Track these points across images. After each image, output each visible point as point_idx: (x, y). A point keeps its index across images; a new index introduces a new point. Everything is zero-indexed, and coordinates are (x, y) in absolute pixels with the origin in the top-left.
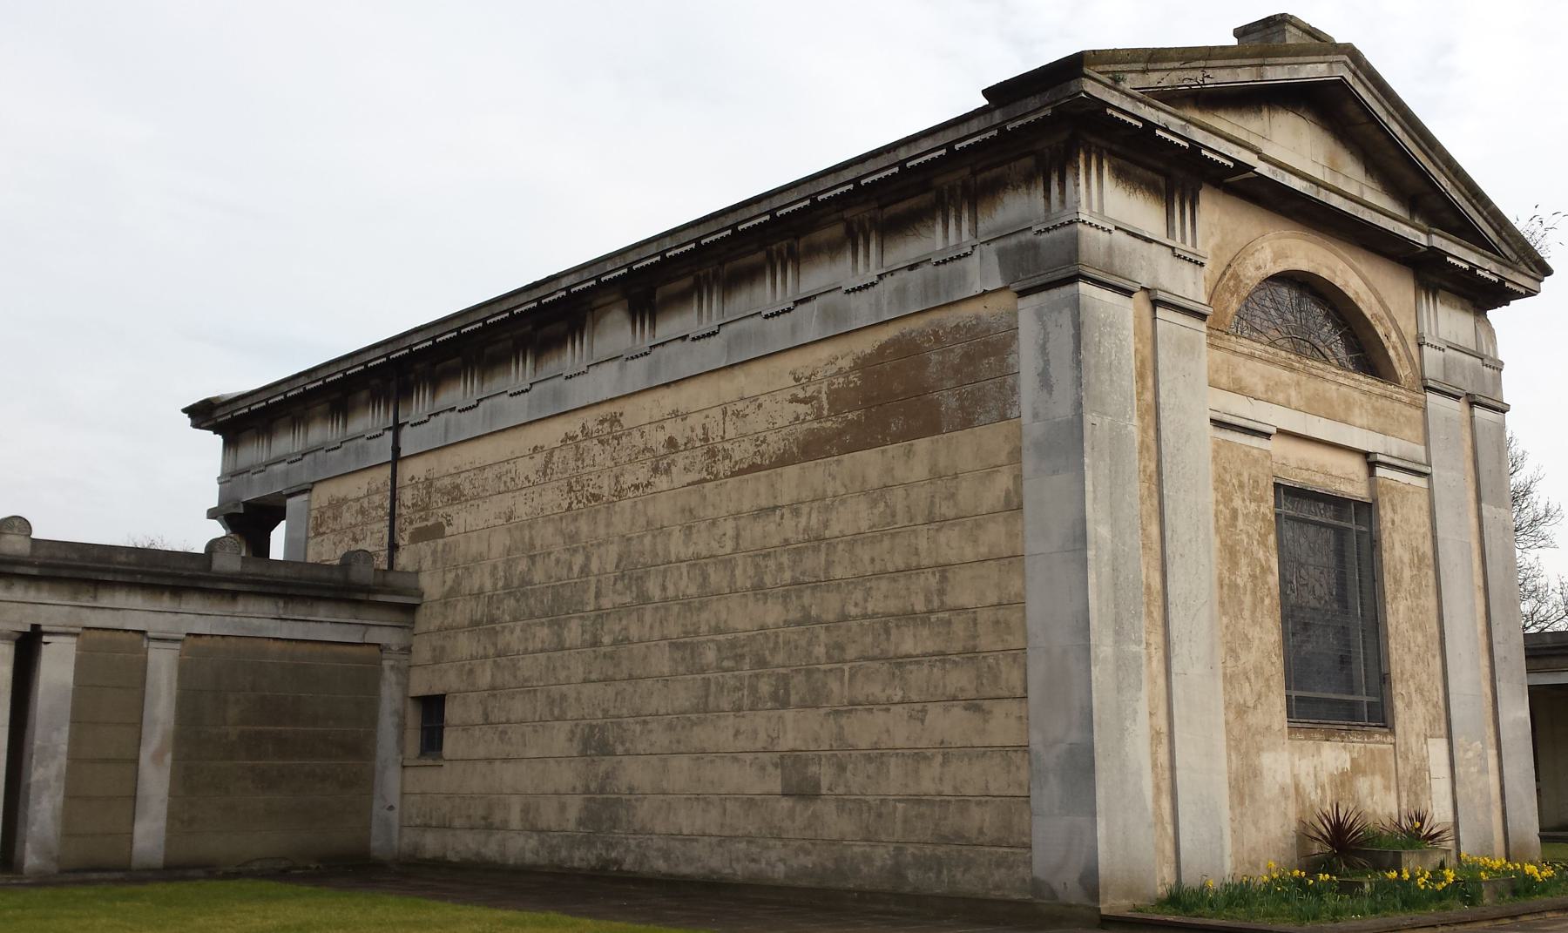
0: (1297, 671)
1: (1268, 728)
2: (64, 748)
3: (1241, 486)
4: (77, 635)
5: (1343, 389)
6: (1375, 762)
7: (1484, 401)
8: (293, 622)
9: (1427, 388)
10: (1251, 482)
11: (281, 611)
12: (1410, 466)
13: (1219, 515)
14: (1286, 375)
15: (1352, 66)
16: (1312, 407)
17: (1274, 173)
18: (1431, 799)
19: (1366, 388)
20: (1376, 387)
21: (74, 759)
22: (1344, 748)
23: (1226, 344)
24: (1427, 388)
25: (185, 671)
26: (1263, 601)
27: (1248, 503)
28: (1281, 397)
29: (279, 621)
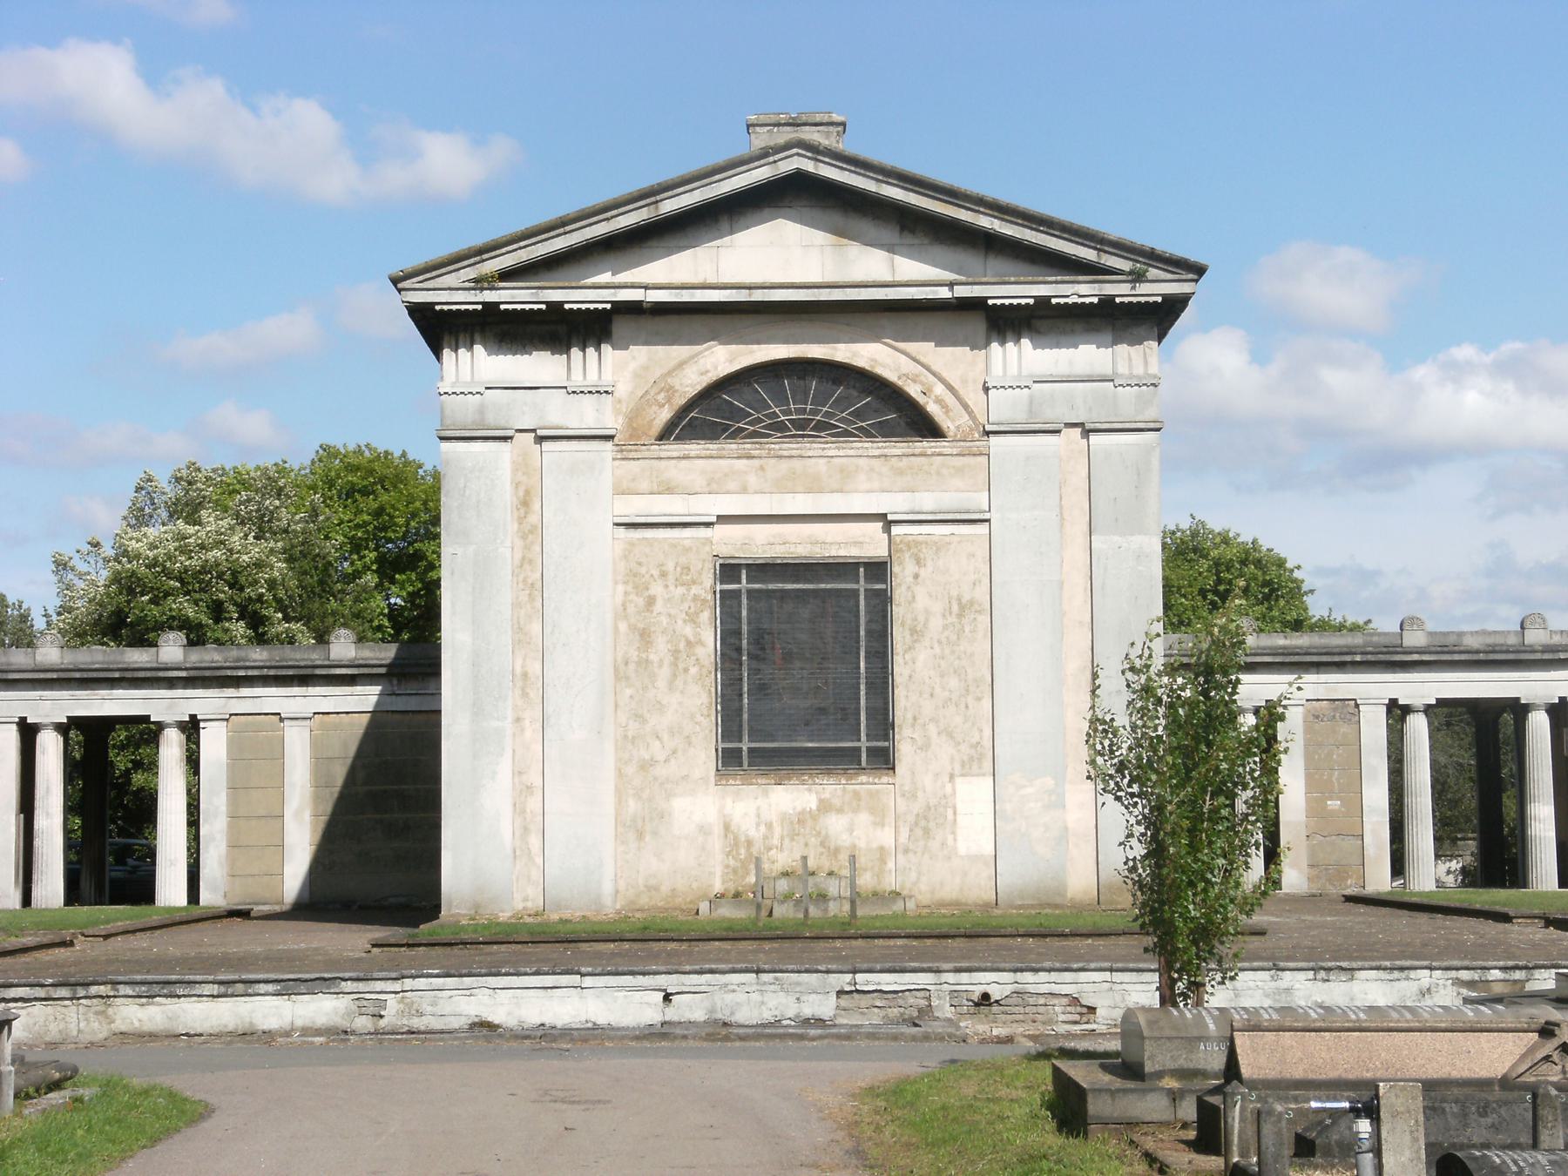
0: (730, 723)
1: (685, 778)
2: (224, 809)
3: (664, 575)
4: (227, 720)
5: (835, 460)
6: (859, 800)
7: (1098, 426)
8: (408, 697)
9: (988, 433)
10: (678, 569)
11: (396, 688)
12: (959, 517)
13: (628, 604)
14: (742, 464)
15: (809, 154)
16: (782, 486)
17: (676, 295)
18: (953, 833)
19: (877, 452)
20: (928, 445)
21: (233, 817)
22: (810, 790)
23: (647, 454)
24: (988, 433)
25: (316, 744)
26: (686, 670)
27: (672, 588)
28: (732, 485)
29: (394, 697)
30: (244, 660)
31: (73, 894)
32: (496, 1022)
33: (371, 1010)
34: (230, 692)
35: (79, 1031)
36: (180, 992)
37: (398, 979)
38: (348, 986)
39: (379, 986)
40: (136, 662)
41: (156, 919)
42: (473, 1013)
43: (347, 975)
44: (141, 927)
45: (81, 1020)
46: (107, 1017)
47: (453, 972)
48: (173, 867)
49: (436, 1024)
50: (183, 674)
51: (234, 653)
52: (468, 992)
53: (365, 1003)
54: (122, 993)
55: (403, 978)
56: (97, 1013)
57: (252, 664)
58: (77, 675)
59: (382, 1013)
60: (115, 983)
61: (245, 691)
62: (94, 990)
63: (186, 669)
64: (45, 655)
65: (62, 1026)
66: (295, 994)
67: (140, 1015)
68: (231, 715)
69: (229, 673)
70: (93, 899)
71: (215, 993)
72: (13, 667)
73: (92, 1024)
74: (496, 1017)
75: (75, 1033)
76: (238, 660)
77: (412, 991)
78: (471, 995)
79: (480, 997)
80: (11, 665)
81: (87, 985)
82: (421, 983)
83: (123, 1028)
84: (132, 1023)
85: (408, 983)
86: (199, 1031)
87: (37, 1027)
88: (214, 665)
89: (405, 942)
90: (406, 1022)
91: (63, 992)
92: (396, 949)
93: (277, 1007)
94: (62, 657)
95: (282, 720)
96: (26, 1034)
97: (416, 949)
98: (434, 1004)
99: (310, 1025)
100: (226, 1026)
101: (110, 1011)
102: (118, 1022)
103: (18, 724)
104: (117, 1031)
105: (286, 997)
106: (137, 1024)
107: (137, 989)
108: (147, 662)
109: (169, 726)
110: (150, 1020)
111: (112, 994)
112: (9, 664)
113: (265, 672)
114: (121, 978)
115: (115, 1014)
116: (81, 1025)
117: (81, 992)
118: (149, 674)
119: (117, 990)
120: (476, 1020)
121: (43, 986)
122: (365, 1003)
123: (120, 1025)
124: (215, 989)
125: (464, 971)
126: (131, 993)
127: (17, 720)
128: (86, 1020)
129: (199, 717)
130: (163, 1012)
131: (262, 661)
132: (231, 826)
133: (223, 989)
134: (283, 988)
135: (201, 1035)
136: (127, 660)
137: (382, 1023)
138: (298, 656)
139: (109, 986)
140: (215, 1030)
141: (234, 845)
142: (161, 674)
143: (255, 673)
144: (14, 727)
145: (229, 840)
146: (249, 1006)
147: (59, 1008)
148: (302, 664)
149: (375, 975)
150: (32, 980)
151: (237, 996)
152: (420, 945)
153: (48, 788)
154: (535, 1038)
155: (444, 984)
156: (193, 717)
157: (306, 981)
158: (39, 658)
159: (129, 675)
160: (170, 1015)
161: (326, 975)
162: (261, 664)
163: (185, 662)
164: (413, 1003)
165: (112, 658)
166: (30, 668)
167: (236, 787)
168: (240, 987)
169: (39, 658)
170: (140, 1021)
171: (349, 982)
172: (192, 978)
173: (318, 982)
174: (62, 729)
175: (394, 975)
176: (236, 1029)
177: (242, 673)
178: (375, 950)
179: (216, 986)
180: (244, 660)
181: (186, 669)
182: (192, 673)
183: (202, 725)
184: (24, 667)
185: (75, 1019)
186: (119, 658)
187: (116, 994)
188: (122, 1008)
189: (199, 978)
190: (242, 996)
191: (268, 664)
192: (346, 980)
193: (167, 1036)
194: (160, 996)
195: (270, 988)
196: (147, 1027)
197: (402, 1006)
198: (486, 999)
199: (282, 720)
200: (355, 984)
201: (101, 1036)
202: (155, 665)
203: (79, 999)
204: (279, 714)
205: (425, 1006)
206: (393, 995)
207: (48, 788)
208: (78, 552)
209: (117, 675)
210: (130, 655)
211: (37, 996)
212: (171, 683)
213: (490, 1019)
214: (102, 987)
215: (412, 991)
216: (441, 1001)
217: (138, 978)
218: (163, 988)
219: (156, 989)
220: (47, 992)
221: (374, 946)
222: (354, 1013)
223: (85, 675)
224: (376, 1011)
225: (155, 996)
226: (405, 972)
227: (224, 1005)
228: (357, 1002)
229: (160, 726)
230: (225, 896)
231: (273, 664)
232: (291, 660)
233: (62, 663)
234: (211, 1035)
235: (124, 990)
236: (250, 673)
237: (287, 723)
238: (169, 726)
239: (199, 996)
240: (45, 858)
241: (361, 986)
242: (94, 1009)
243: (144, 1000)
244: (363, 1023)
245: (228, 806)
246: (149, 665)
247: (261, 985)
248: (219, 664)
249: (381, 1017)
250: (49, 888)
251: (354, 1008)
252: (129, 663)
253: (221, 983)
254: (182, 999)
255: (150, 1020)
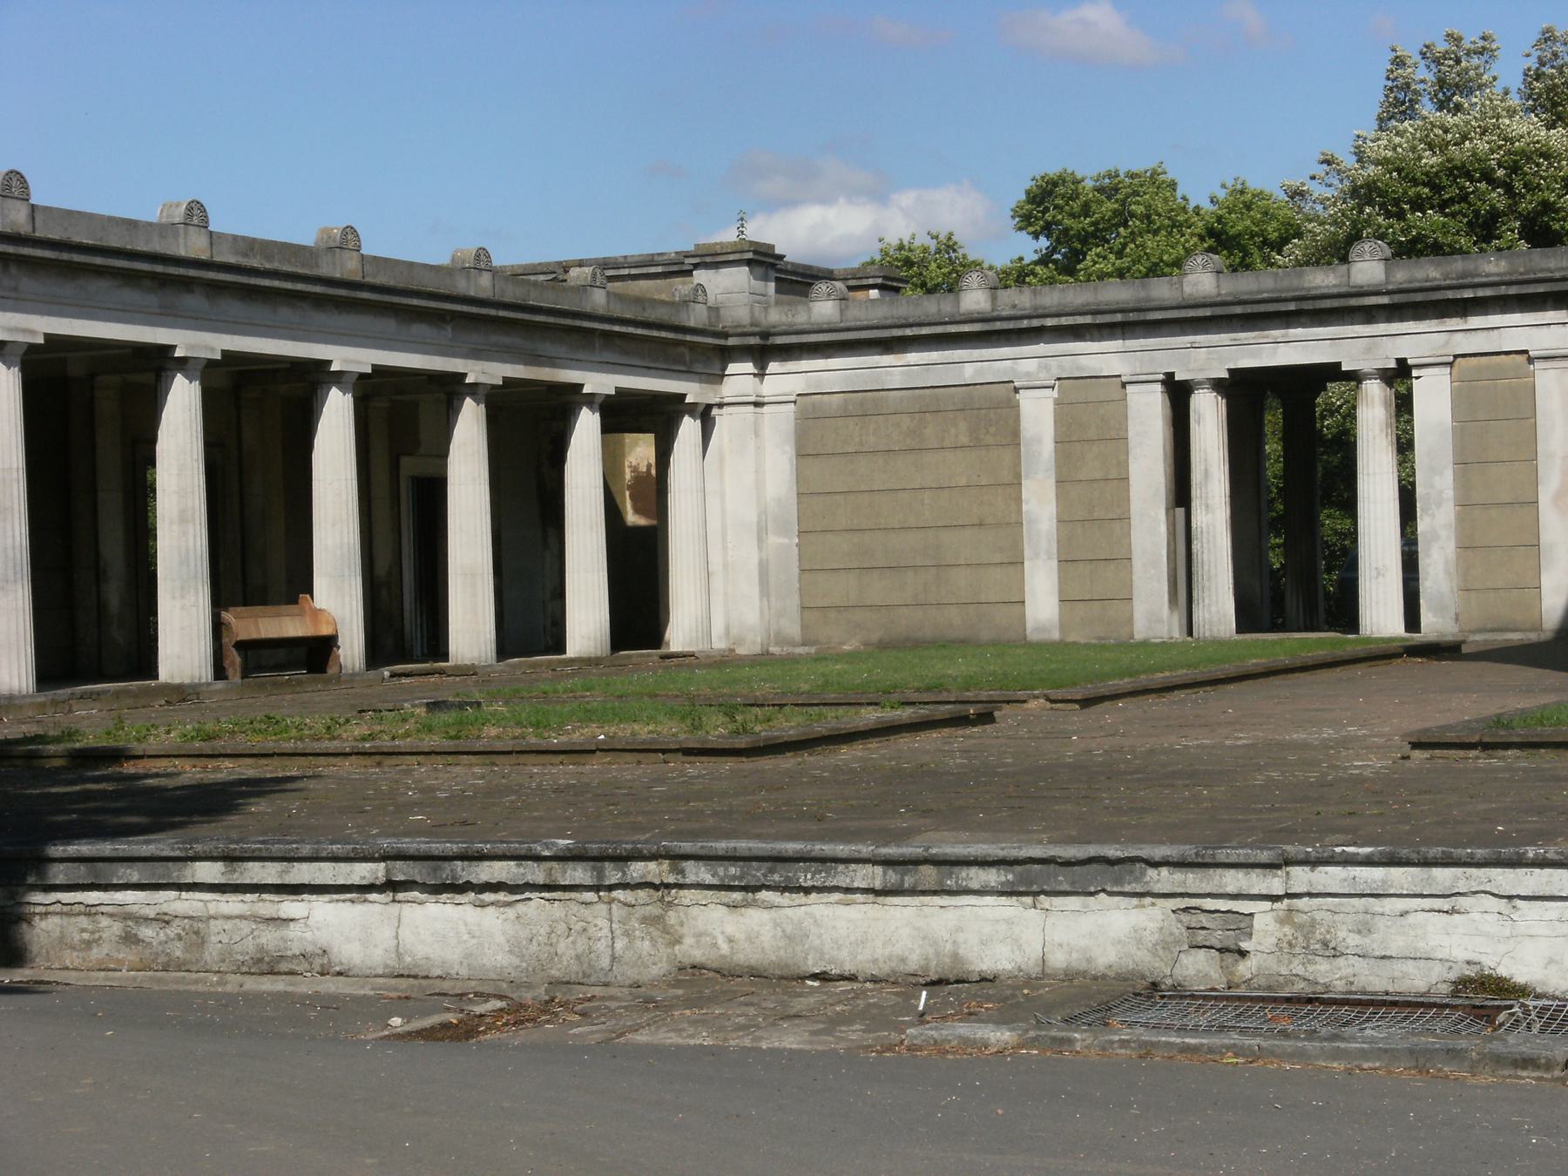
2: (1449, 493)
4: (1451, 364)
30: (1473, 276)
31: (1248, 618)
32: (1520, 978)
33: (1217, 938)
34: (1454, 323)
35: (613, 958)
36: (806, 879)
37: (1277, 866)
38: (1163, 879)
39: (1233, 880)
40: (1320, 287)
41: (1360, 650)
42: (1461, 955)
43: (1159, 852)
44: (1206, 677)
45: (618, 932)
46: (666, 930)
47: (1404, 852)
48: (1381, 579)
49: (1374, 979)
50: (1385, 300)
51: (1457, 265)
52: (1444, 904)
53: (1204, 920)
54: (691, 878)
55: (1289, 862)
56: (644, 920)
57: (1484, 280)
58: (1238, 310)
59: (1244, 945)
60: (677, 858)
61: (1475, 321)
62: (637, 870)
63: (1388, 293)
64: (1196, 284)
65: (581, 946)
66: (1047, 893)
67: (730, 929)
68: (1456, 357)
69: (1450, 295)
70: (1301, 623)
71: (878, 885)
72: (1153, 304)
73: (638, 943)
74: (1521, 967)
75: (605, 962)
76: (1464, 275)
77: (1310, 895)
78: (1452, 911)
79: (1476, 916)
80: (1154, 300)
81: (623, 859)
82: (1331, 877)
83: (698, 955)
84: (715, 945)
85: (1301, 877)
86: (849, 968)
87: (534, 947)
88: (1428, 284)
89: (1476, 739)
90: (1300, 970)
91: (578, 874)
92: (1461, 753)
93: (1009, 922)
94: (1218, 286)
95: (1531, 360)
96: (516, 961)
97: (1501, 753)
98: (1364, 929)
99: (1083, 966)
100: (903, 960)
101: (672, 917)
102: (689, 941)
103: (1163, 382)
104: (687, 961)
105: (1028, 900)
106: (725, 948)
107: (721, 871)
108: (1334, 286)
109: (1368, 376)
110: (749, 939)
111: (671, 879)
112: (1148, 300)
113: (1503, 290)
114: (687, 847)
115: (682, 924)
116: (619, 945)
117: (613, 875)
118: (1336, 303)
119: (682, 872)
120: (1471, 972)
121: (538, 858)
122: (1204, 920)
123: (691, 950)
124: (874, 876)
125: (1435, 851)
126: (708, 878)
127: (1161, 377)
128: (627, 934)
129: (1409, 362)
130: (776, 924)
131: (1498, 275)
132: (1461, 519)
133: (893, 877)
134: (1021, 879)
135: (852, 978)
136: (1306, 285)
137: (1245, 969)
138: (1552, 264)
139: (666, 864)
140: (881, 970)
141: (1467, 546)
142: (1353, 302)
143: (1488, 292)
144: (1158, 387)
145: (1458, 539)
146: (950, 917)
147: (575, 907)
148: (1557, 275)
149: (1222, 855)
150: (523, 848)
151: (924, 893)
152: (1507, 746)
153: (1206, 470)
154: (1549, 1066)
155: (1384, 882)
156: (1401, 362)
157: (1068, 863)
158: (1187, 289)
159: (1308, 305)
160: (789, 929)
161: (1112, 852)
162: (1496, 279)
163: (1388, 282)
164: (1313, 924)
165: (1286, 283)
166: (1174, 303)
167: (1467, 462)
168: (928, 874)
169: (1187, 289)
170: (730, 940)
171: (1164, 871)
172: (828, 849)
173: (1094, 866)
174: (1218, 385)
175: (1264, 856)
176: (926, 969)
177: (1468, 294)
178: (1418, 755)
179: (879, 870)
180: (1473, 276)
181: (1388, 293)
182: (1398, 298)
183: (1415, 373)
184: (1167, 303)
185: (606, 931)
186: (1295, 283)
187: (681, 881)
188: (695, 911)
189: (841, 849)
190: (935, 893)
191: (1506, 278)
192: (1156, 864)
193: (782, 978)
194: (769, 888)
195: (992, 877)
196: (746, 955)
197: (1287, 929)
198: (1491, 924)
199: (1531, 360)
200: (1178, 876)
201: (656, 971)
202: (1343, 290)
203: (611, 888)
204: (1526, 352)
205: (1342, 934)
206: (1267, 905)
207: (1206, 470)
208: (1328, 162)
209: (1292, 307)
210: (1311, 277)
211: (530, 878)
212: (1369, 315)
213: (1503, 971)
214: (652, 865)
215: (1310, 895)
216: (1381, 923)
217: (721, 846)
218: (772, 871)
219: (758, 873)
220: (549, 872)
221: (1416, 745)
222: (1178, 942)
223: (1249, 309)
224: (1228, 939)
225: (756, 889)
226: (1291, 849)
227: (896, 912)
228: (1185, 918)
229: (1355, 377)
230: (1457, 619)
231: (1514, 277)
232: (1542, 270)
233: (1219, 295)
234: (875, 980)
235: (697, 872)
236: (1481, 293)
237: (1538, 365)
238: (1368, 376)
239: (848, 890)
240: (1206, 568)
241: (1192, 880)
242: (640, 912)
243: (737, 896)
244: (1198, 968)
245: (1455, 489)
246: (1335, 291)
247: (974, 871)
248: (1436, 283)
249: (1243, 954)
250: (1214, 609)
251: (1178, 930)
252: (1309, 289)
253: (887, 863)
254: (814, 895)
255: (749, 939)
